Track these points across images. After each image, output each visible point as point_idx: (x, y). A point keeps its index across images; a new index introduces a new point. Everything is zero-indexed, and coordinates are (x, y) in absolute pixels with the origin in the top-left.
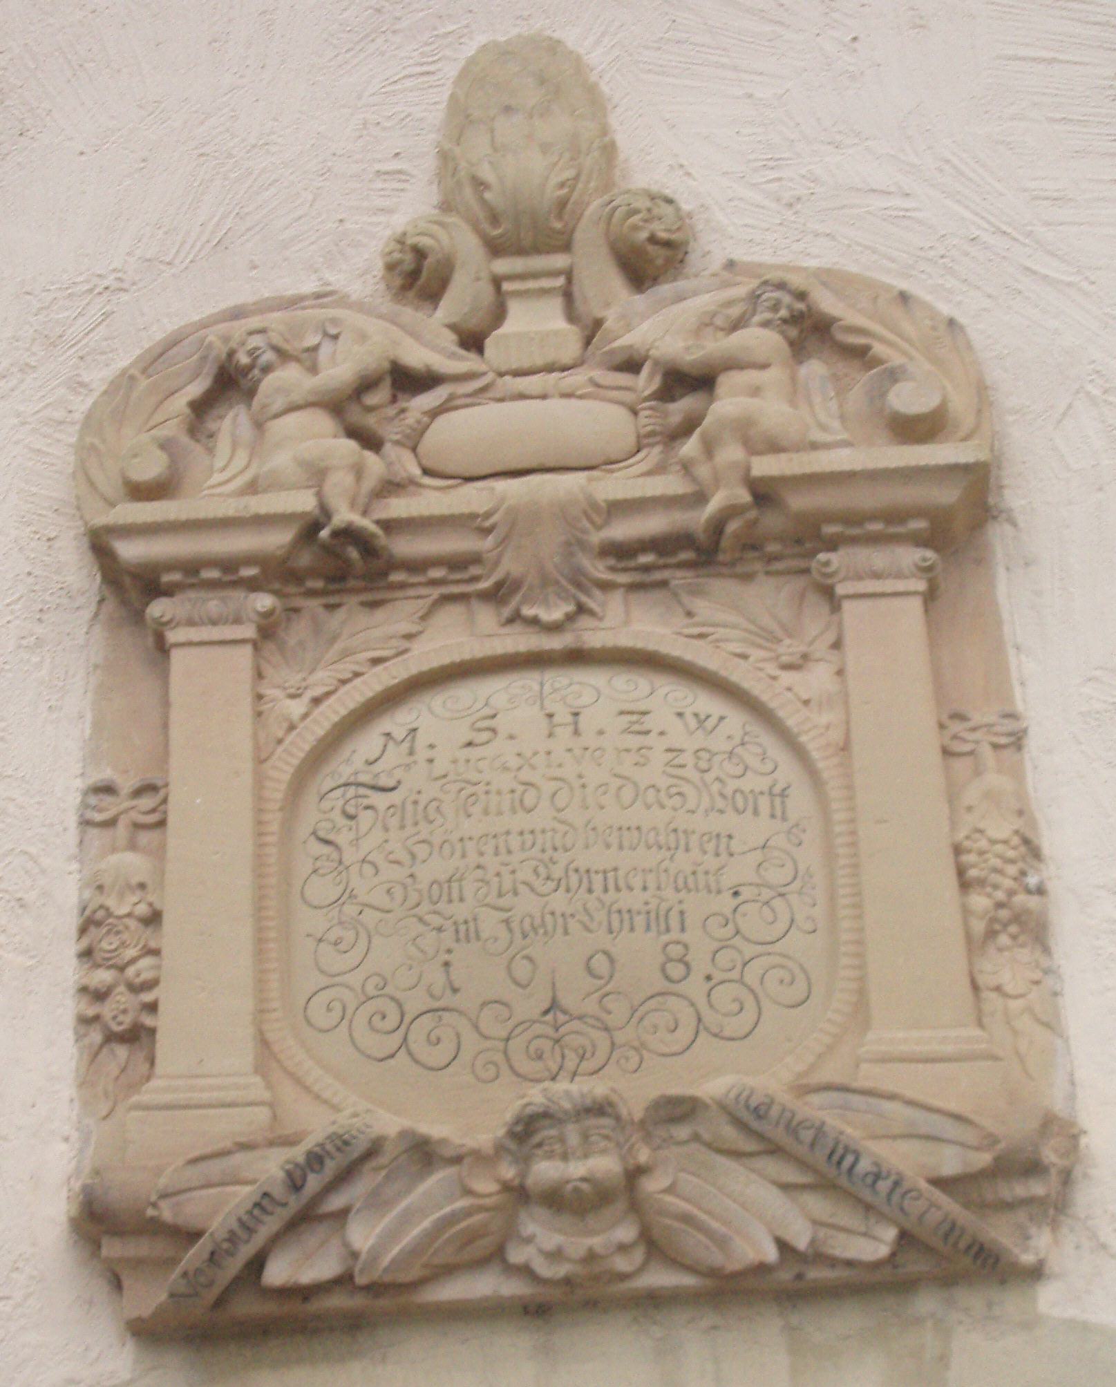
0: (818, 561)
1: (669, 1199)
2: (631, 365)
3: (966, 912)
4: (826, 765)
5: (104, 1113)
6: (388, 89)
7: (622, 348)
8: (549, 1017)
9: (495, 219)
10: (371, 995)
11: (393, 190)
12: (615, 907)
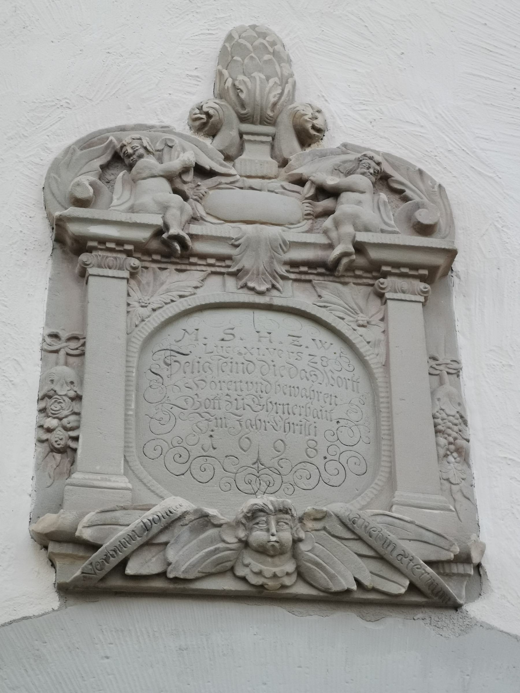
0: (379, 282)
1: (310, 554)
2: (301, 182)
3: (438, 444)
4: (378, 372)
5: (49, 484)
6: (193, 38)
7: (298, 174)
8: (255, 466)
9: (243, 105)
10: (175, 446)
11: (194, 84)
12: (287, 421)
